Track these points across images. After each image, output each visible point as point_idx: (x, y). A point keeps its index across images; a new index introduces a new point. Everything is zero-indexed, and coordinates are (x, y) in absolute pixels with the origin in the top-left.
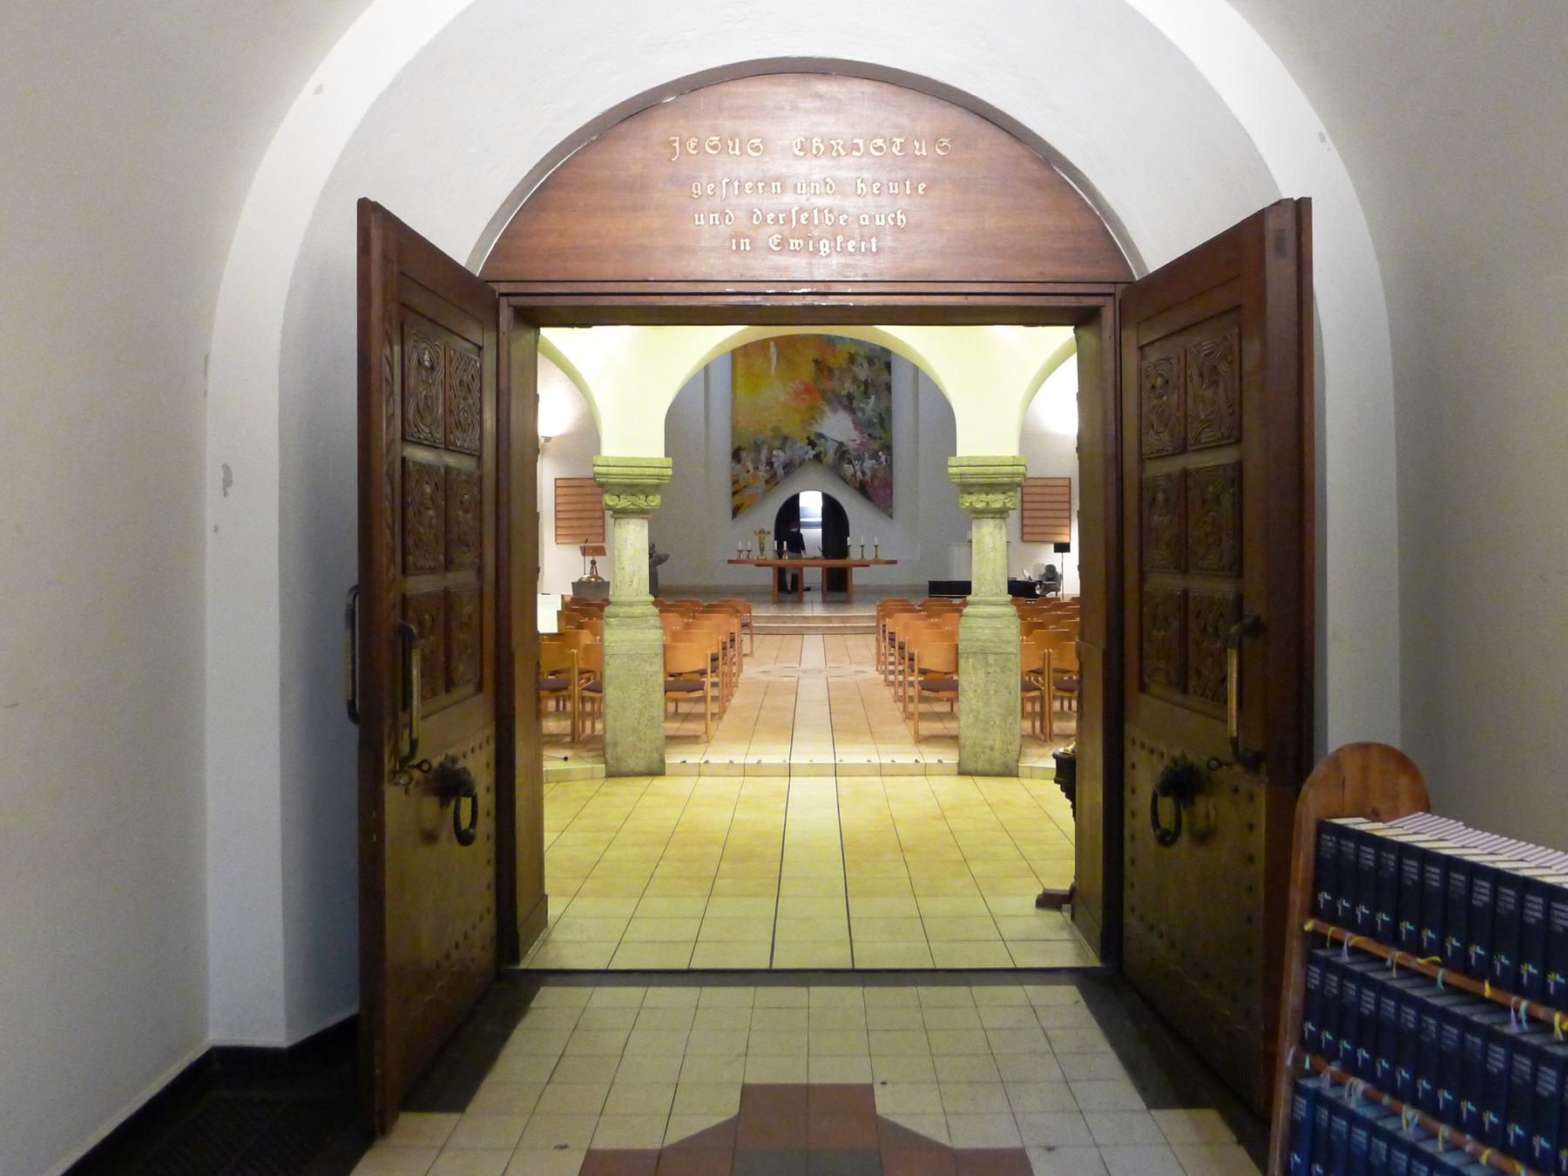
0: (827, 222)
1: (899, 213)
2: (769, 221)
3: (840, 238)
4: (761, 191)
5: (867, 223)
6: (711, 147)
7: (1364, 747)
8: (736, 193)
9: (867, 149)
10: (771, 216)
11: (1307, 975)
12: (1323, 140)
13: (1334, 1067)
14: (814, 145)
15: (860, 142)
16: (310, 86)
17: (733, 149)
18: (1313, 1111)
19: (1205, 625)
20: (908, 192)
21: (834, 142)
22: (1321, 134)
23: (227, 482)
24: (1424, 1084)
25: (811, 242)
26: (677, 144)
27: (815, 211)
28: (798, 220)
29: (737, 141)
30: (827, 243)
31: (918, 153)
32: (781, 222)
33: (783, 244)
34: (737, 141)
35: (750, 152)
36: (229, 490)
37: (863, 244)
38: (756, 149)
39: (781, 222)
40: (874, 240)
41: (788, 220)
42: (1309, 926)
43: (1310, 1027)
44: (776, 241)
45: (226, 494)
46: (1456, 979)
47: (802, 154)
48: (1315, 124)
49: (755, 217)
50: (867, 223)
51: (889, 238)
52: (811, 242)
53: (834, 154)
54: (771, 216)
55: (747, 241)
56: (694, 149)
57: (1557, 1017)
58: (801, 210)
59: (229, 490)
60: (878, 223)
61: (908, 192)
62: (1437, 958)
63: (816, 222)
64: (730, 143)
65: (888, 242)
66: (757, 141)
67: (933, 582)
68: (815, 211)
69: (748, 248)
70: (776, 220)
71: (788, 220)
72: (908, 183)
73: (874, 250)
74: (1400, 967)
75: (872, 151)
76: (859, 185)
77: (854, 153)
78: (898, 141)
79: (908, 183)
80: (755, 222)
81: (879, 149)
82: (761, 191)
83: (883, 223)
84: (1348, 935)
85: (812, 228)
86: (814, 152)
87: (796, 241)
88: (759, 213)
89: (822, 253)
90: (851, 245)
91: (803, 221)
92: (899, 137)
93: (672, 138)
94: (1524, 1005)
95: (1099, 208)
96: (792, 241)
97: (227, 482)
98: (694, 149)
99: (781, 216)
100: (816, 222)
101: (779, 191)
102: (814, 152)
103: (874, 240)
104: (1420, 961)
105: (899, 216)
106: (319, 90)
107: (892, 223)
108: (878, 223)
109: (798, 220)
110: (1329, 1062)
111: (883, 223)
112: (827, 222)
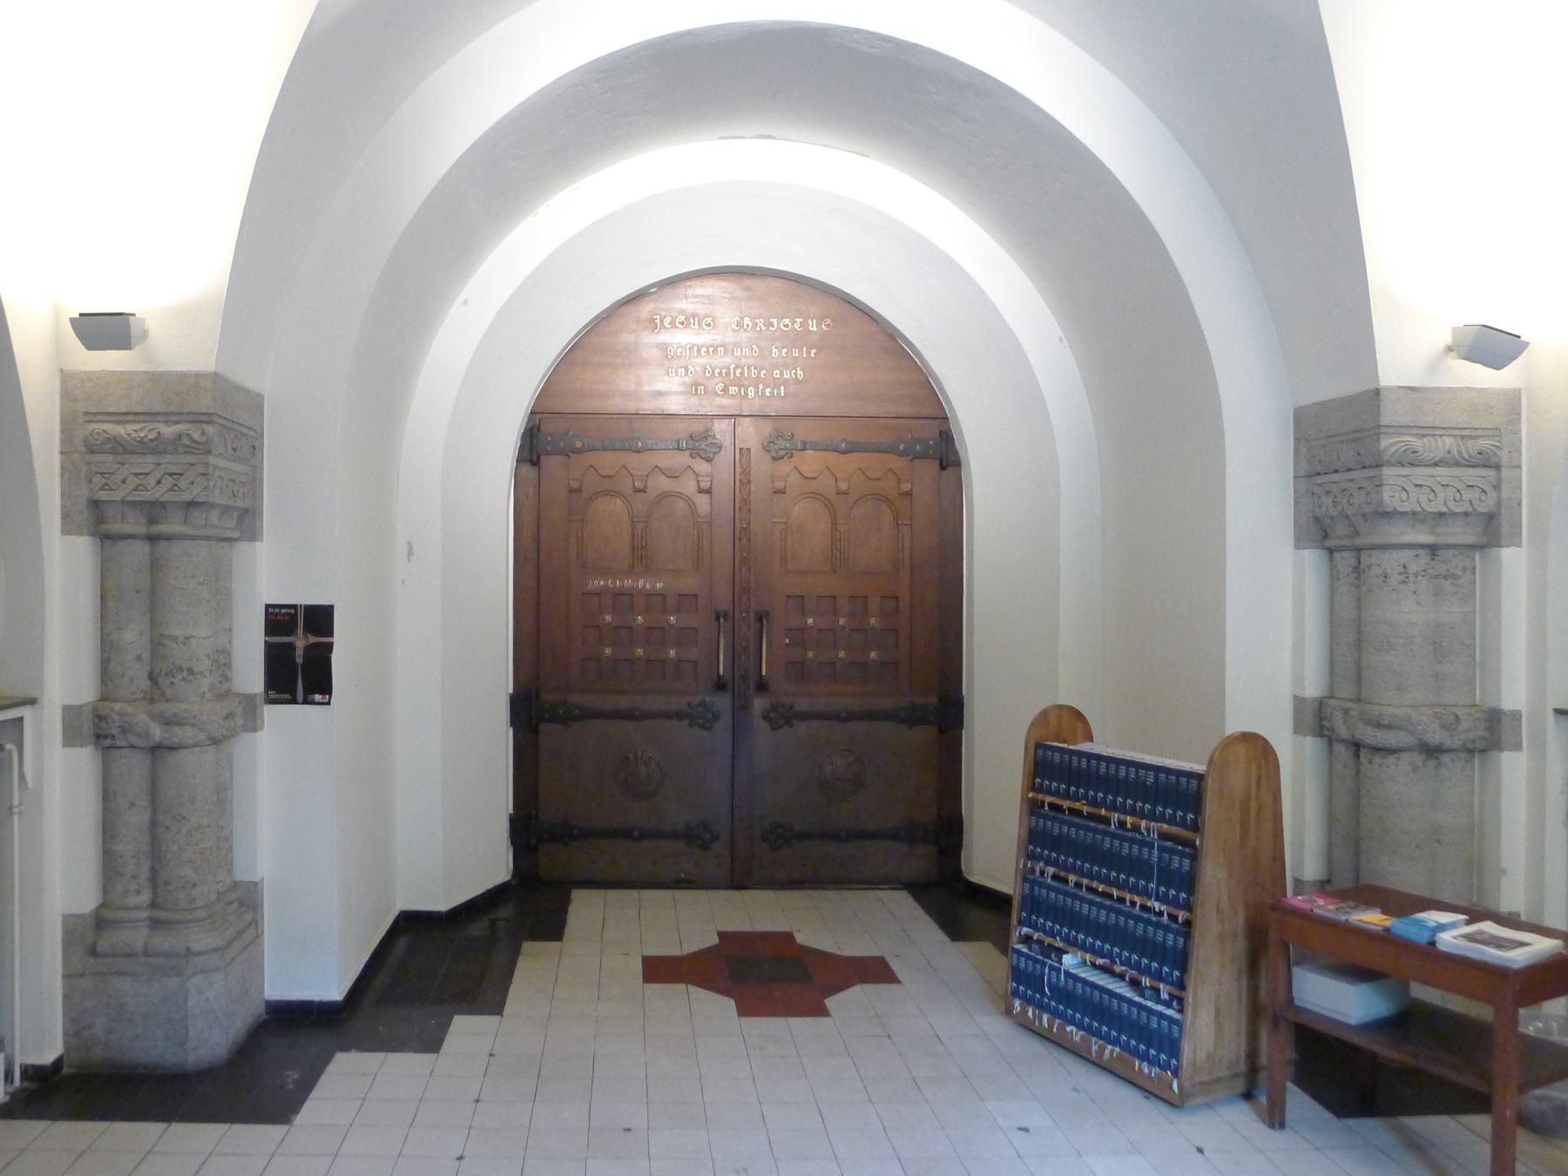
0: (753, 375)
1: (798, 369)
2: (716, 374)
3: (761, 387)
4: (711, 354)
5: (778, 376)
6: (680, 323)
7: (1060, 707)
8: (696, 355)
9: (778, 325)
10: (717, 371)
11: (1030, 822)
12: (1061, 341)
13: (1041, 864)
14: (745, 323)
15: (775, 321)
16: (459, 302)
17: (694, 324)
18: (1032, 889)
19: (1480, 477)
20: (805, 355)
21: (757, 321)
22: (1061, 338)
23: (410, 553)
24: (1153, 1052)
25: (742, 389)
26: (658, 321)
27: (746, 368)
28: (734, 374)
29: (696, 319)
30: (753, 389)
31: (811, 329)
32: (724, 375)
33: (725, 390)
34: (696, 319)
35: (704, 326)
36: (411, 558)
37: (776, 390)
38: (709, 325)
39: (724, 375)
40: (782, 388)
41: (728, 374)
42: (1030, 795)
43: (1031, 847)
44: (721, 388)
45: (409, 560)
46: (1091, 810)
47: (737, 328)
48: (1058, 332)
49: (707, 371)
50: (778, 376)
51: (792, 386)
52: (742, 389)
53: (758, 329)
54: (717, 371)
55: (702, 388)
56: (669, 324)
57: (1128, 818)
58: (737, 367)
59: (411, 558)
60: (785, 376)
61: (805, 355)
62: (1085, 802)
63: (746, 375)
64: (692, 321)
65: (792, 389)
66: (709, 320)
67: (1518, 750)
68: (746, 368)
69: (703, 392)
70: (720, 373)
71: (728, 374)
72: (805, 349)
73: (783, 394)
74: (1069, 809)
75: (782, 327)
76: (774, 350)
77: (771, 328)
78: (798, 320)
79: (805, 349)
80: (707, 374)
81: (786, 326)
82: (711, 354)
83: (788, 376)
84: (1048, 797)
85: (743, 379)
86: (745, 327)
87: (734, 388)
88: (709, 368)
89: (749, 397)
90: (768, 390)
91: (738, 375)
92: (799, 318)
93: (655, 317)
94: (1116, 815)
95: (925, 366)
96: (730, 388)
97: (410, 553)
98: (669, 324)
99: (724, 371)
100: (746, 375)
101: (723, 354)
102: (745, 327)
103: (782, 388)
104: (1077, 804)
105: (799, 372)
106: (465, 302)
107: (794, 376)
108: (785, 376)
109: (734, 374)
110: (1039, 862)
111: (788, 376)
112: (753, 375)
